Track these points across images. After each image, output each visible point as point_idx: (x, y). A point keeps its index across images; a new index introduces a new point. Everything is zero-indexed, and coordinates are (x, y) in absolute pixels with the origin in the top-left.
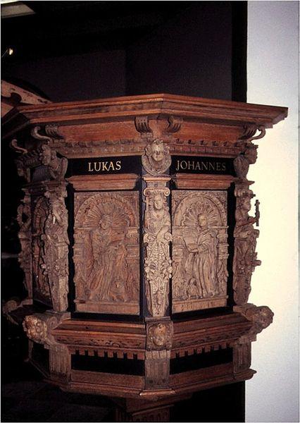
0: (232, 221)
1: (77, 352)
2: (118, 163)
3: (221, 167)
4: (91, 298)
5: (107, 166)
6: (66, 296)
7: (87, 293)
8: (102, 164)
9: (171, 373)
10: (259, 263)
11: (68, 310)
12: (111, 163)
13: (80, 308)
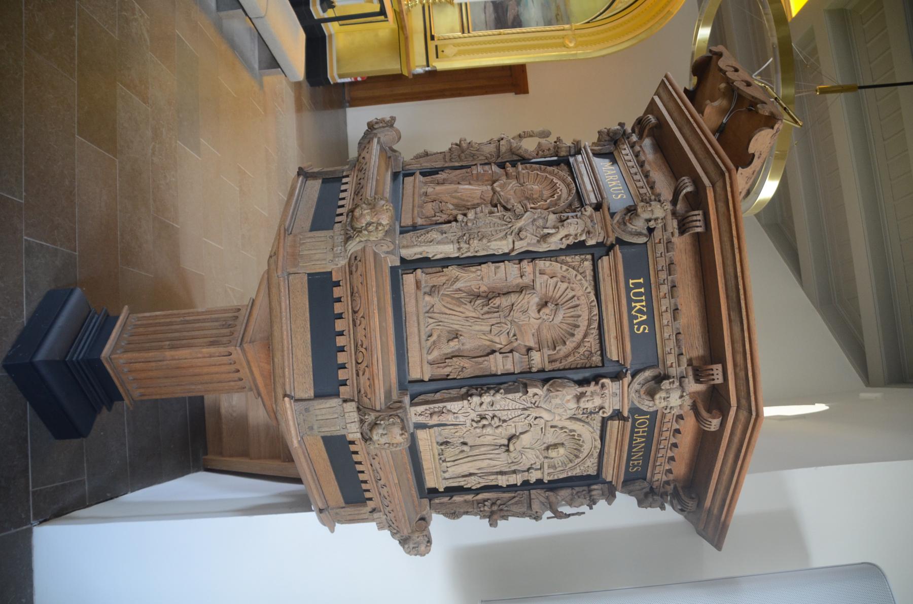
0: (554, 486)
1: (337, 284)
2: (645, 329)
3: (634, 466)
4: (427, 298)
5: (640, 311)
6: (424, 255)
7: (433, 290)
8: (641, 301)
9: (324, 438)
10: (493, 524)
11: (403, 260)
12: (645, 317)
13: (409, 280)
